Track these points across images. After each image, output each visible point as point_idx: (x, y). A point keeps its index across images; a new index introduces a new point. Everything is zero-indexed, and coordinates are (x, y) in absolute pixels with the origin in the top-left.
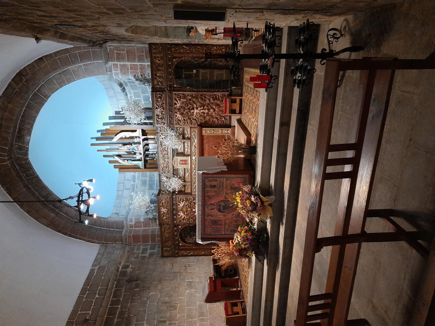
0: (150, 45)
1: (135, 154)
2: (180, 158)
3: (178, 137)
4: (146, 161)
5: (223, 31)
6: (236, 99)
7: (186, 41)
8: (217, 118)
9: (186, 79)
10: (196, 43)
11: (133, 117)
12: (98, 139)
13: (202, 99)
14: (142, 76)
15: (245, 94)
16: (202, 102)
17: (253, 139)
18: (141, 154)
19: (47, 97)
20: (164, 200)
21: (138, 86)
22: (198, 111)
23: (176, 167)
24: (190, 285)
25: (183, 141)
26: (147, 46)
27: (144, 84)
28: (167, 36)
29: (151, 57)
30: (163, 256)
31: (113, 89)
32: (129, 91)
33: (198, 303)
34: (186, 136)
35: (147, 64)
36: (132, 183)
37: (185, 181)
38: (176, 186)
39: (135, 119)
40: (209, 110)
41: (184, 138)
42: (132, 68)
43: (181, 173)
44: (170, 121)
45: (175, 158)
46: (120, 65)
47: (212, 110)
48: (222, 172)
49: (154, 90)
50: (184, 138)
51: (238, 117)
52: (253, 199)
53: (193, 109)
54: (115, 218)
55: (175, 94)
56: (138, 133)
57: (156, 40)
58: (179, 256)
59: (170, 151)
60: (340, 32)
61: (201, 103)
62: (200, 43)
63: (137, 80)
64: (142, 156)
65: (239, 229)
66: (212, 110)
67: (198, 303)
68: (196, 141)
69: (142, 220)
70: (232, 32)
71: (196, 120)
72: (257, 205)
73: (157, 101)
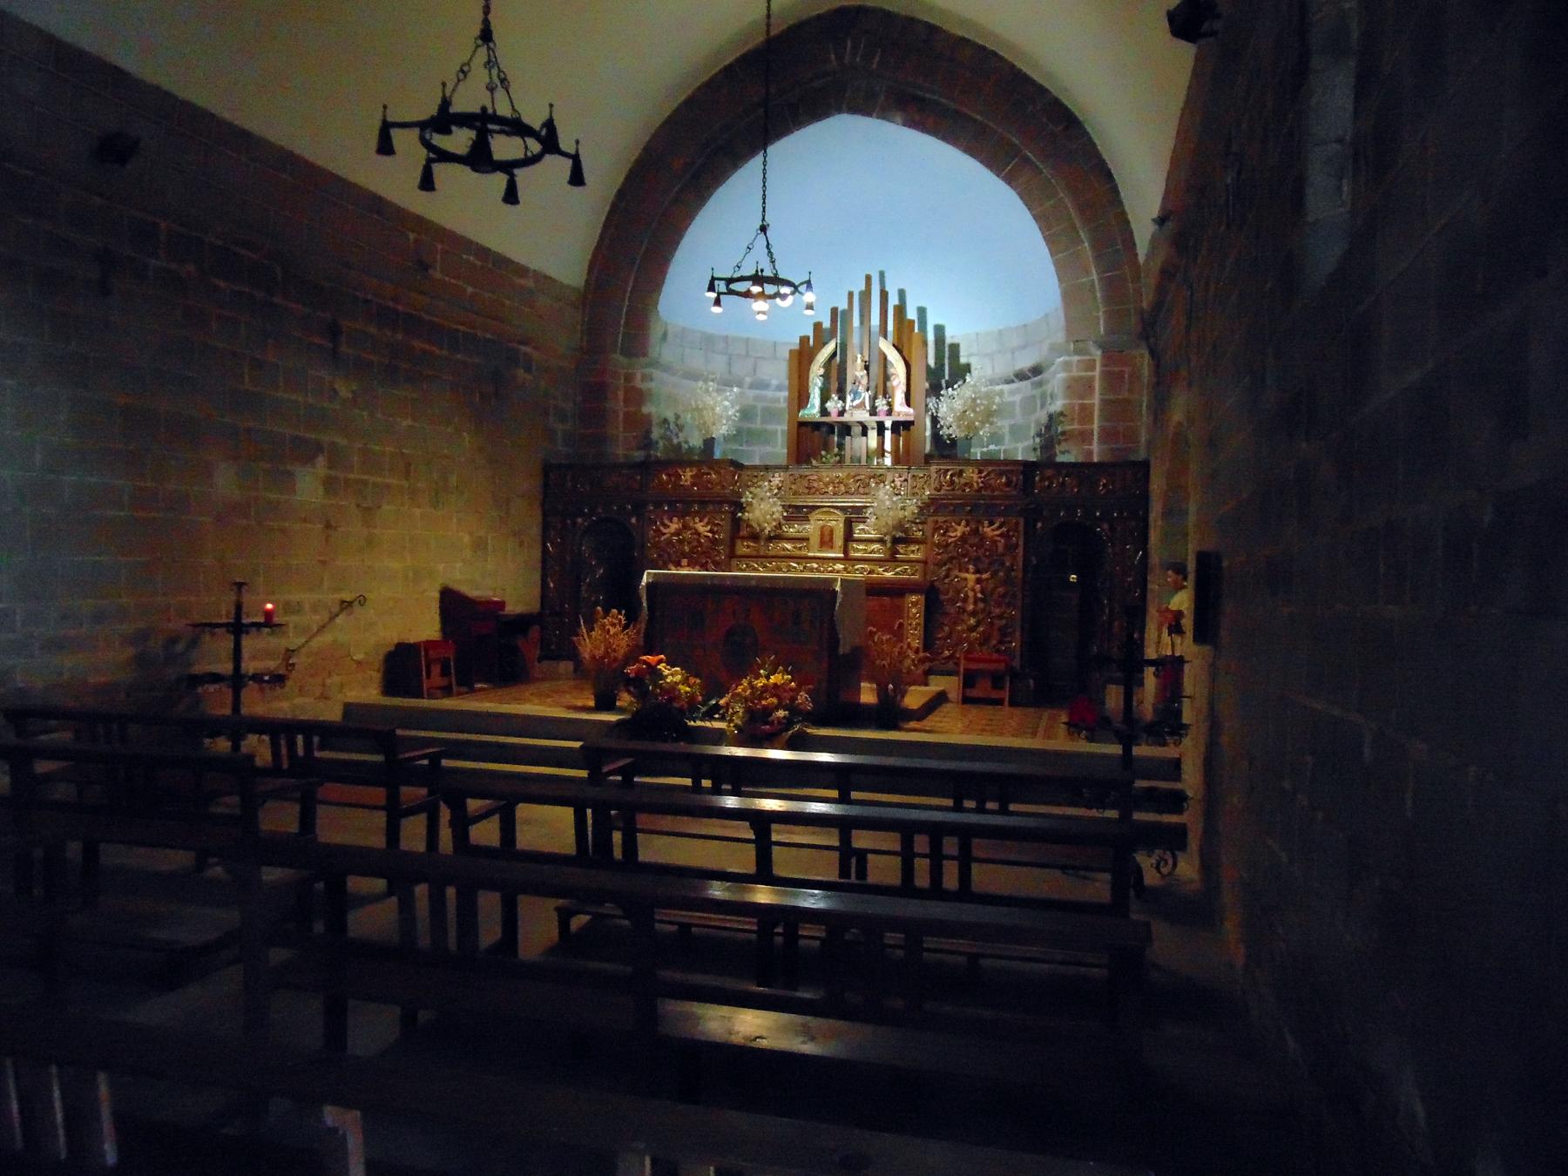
0: (1145, 466)
1: (842, 398)
2: (837, 524)
3: (900, 526)
4: (816, 426)
5: (1178, 654)
6: (1002, 688)
7: (1155, 559)
8: (949, 636)
9: (1047, 545)
10: (1150, 586)
11: (958, 405)
12: (900, 310)
13: (1004, 596)
14: (1063, 433)
15: (1018, 712)
16: (995, 597)
17: (913, 724)
18: (841, 413)
19: (1009, 180)
20: (713, 483)
21: (1034, 417)
22: (971, 584)
23: (814, 516)
24: (479, 545)
25: (887, 538)
26: (1141, 455)
27: (1039, 435)
28: (1168, 513)
29: (1113, 465)
30: (547, 469)
31: (1024, 347)
32: (1018, 390)
33: (441, 567)
34: (901, 548)
35: (1096, 452)
36: (748, 380)
37: (770, 539)
38: (757, 513)
39: (950, 407)
40: (974, 614)
41: (896, 541)
42: (1083, 408)
43: (792, 530)
44: (946, 506)
45: (841, 517)
46: (1092, 379)
47: (972, 621)
48: (834, 641)
49: (1028, 467)
50: (896, 541)
51: (954, 695)
52: (781, 713)
53: (977, 571)
54: (655, 332)
55: (1017, 524)
56: (902, 410)
57: (1157, 484)
58: (545, 515)
59: (857, 501)
60: (1170, 874)
61: (992, 594)
62: (1149, 596)
63: (1051, 417)
64: (834, 418)
65: (692, 680)
66: (972, 621)
67: (441, 567)
68: (889, 575)
69: (645, 410)
70: (1171, 668)
71: (947, 576)
72: (766, 723)
73: (1000, 474)
